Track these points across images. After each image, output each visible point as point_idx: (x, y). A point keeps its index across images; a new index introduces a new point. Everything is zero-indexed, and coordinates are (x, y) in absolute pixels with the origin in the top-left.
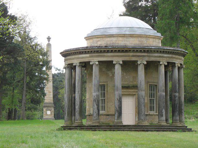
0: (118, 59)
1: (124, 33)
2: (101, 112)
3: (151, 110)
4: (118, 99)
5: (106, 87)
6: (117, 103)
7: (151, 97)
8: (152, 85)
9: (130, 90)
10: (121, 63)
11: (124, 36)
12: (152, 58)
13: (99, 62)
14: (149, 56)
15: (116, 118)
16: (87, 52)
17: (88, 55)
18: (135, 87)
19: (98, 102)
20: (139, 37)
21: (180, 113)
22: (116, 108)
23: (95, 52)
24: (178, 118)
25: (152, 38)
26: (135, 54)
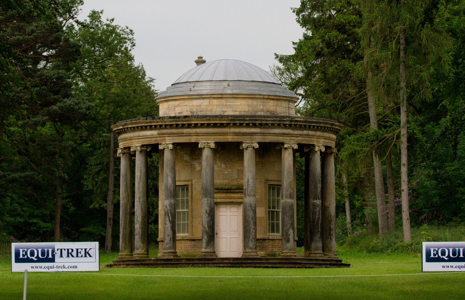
0: (207, 141)
1: (221, 92)
2: (179, 235)
3: (273, 231)
4: (208, 211)
5: (190, 189)
6: (205, 219)
7: (274, 207)
8: (273, 185)
9: (232, 195)
10: (213, 146)
11: (221, 96)
12: (270, 137)
13: (174, 144)
14: (263, 134)
15: (204, 245)
16: (153, 127)
17: (155, 132)
18: (239, 189)
19: (172, 217)
20: (250, 98)
21: (326, 235)
22: (204, 227)
23: (168, 127)
24: (320, 245)
25: (273, 99)
26: (285, 131)
